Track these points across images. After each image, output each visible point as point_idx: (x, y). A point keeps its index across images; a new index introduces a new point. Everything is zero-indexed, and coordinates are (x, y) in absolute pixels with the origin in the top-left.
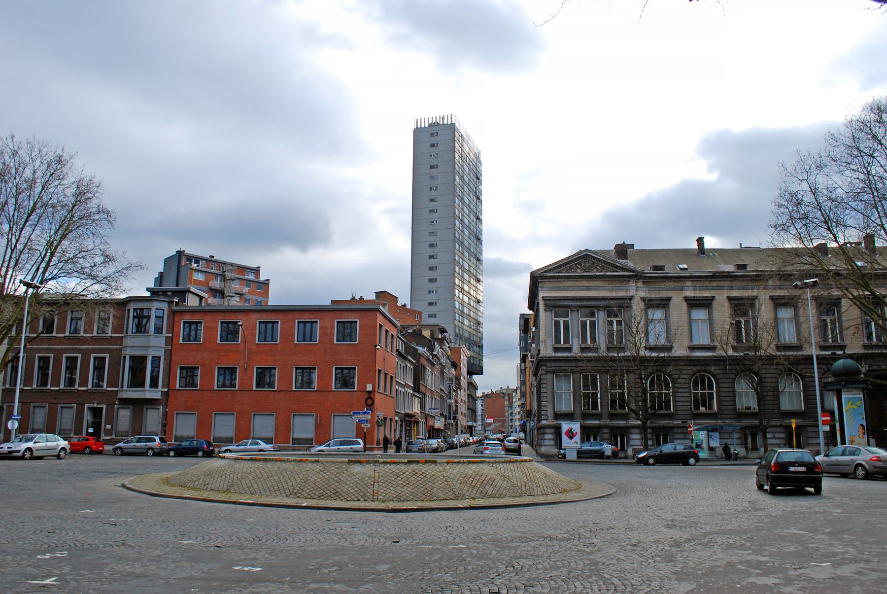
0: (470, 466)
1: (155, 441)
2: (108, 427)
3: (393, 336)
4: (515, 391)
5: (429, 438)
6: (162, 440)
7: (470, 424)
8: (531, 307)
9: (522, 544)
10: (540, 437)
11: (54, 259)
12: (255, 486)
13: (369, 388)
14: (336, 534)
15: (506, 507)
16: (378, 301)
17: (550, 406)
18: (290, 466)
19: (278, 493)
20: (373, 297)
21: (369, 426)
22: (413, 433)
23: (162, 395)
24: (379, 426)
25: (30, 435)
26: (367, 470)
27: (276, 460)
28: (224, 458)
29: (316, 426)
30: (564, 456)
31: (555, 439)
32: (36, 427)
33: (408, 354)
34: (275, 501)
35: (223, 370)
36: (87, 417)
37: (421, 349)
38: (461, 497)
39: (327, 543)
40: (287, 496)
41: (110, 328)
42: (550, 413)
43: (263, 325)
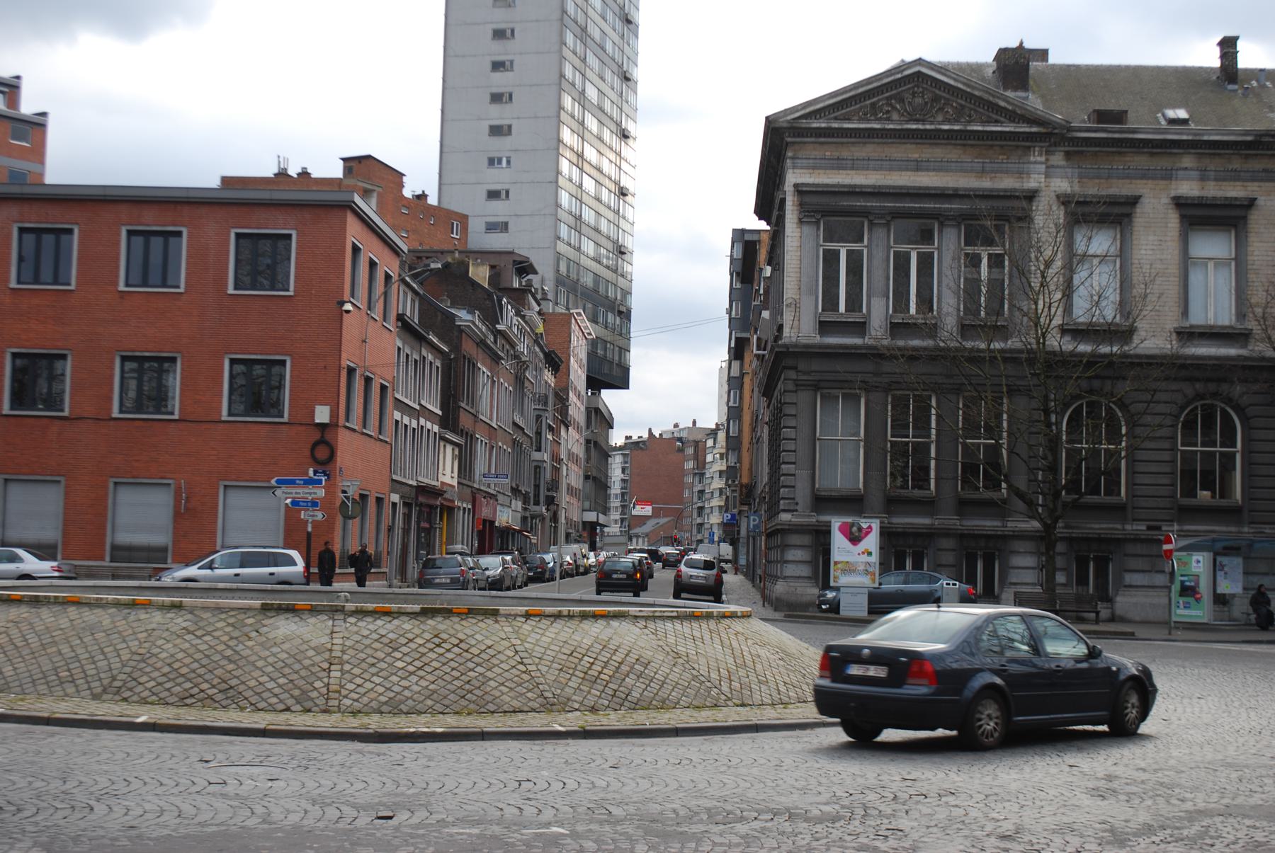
0: (586, 625)
3: (388, 277)
4: (713, 433)
5: (482, 551)
7: (591, 516)
8: (763, 209)
10: (775, 555)
13: (322, 414)
18: (104, 618)
20: (337, 171)
21: (319, 516)
22: (439, 538)
24: (347, 517)
29: (178, 515)
30: (835, 607)
31: (813, 563)
33: (428, 328)
34: (62, 709)
38: (563, 706)
40: (95, 697)
42: (802, 494)
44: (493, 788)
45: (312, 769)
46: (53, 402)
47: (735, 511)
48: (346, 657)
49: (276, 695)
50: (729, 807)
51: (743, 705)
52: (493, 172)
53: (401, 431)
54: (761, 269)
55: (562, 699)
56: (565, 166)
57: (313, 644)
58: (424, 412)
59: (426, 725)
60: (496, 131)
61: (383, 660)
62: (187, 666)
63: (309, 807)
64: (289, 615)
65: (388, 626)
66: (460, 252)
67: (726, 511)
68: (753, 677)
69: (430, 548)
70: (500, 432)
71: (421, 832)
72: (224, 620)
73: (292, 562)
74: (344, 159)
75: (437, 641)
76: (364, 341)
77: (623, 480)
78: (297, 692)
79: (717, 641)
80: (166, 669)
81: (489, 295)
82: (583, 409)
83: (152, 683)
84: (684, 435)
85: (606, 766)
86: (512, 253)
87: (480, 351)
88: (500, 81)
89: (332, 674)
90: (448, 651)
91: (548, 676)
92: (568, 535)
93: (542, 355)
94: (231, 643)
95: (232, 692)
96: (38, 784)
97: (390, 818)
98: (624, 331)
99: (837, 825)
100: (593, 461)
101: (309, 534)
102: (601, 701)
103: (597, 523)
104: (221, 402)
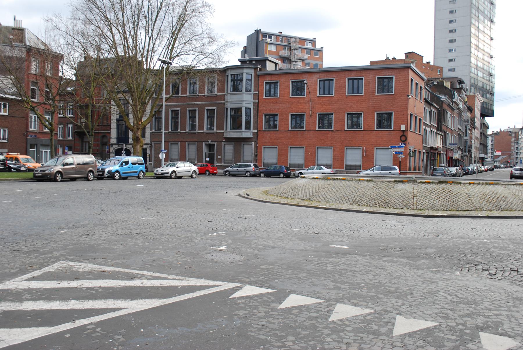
0: (488, 186)
1: (250, 166)
2: (219, 157)
3: (421, 87)
5: (449, 166)
6: (255, 166)
7: (482, 156)
11: (177, 42)
12: (328, 197)
13: (403, 128)
15: (516, 217)
16: (407, 60)
18: (352, 183)
19: (345, 202)
20: (403, 57)
21: (403, 156)
22: (437, 162)
24: (410, 157)
25: (173, 163)
26: (408, 188)
27: (342, 180)
28: (304, 177)
29: (363, 157)
32: (173, 157)
33: (433, 102)
34: (344, 207)
35: (295, 116)
36: (205, 150)
37: (443, 97)
38: (482, 210)
40: (351, 204)
41: (216, 89)
43: (322, 83)
52: (451, 53)
53: (425, 132)
56: (473, 50)
58: (432, 126)
60: (451, 41)
69: (434, 165)
73: (396, 169)
74: (406, 54)
77: (492, 145)
78: (405, 204)
81: (450, 91)
82: (479, 123)
84: (511, 130)
86: (457, 78)
88: (452, 26)
92: (475, 161)
100: (483, 139)
101: (400, 162)
103: (484, 158)
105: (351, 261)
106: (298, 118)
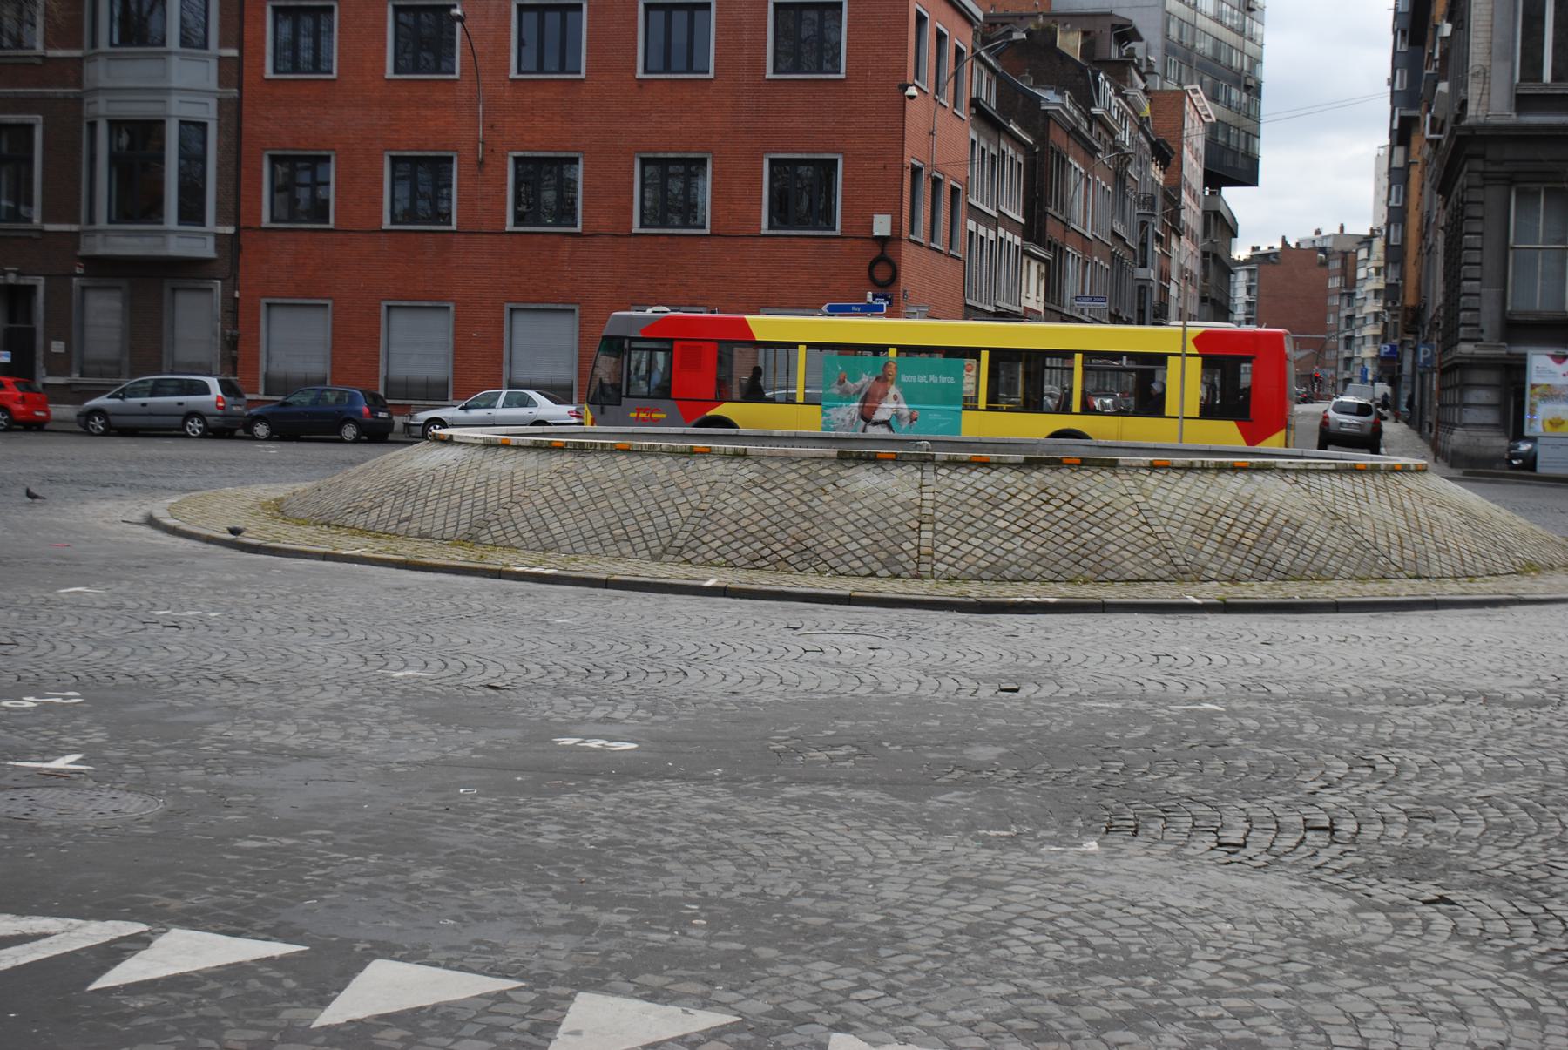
1: (205, 390)
2: (58, 347)
3: (959, 52)
4: (1367, 241)
6: (227, 388)
9: (1396, 710)
12: (555, 527)
13: (882, 226)
14: (825, 664)
17: (1490, 295)
18: (659, 468)
19: (627, 549)
23: (218, 246)
28: (449, 441)
30: (1530, 462)
31: (1501, 407)
34: (622, 571)
37: (1050, 98)
38: (1198, 575)
39: (805, 685)
40: (655, 558)
42: (1489, 318)
43: (531, 17)
44: (1128, 663)
45: (915, 639)
46: (565, 212)
47: (1396, 342)
48: (938, 515)
49: (859, 558)
50: (1410, 688)
51: (1418, 577)
53: (976, 244)
54: (1437, 27)
55: (1195, 567)
57: (899, 500)
58: (1003, 220)
59: (1035, 594)
61: (981, 519)
62: (756, 523)
63: (922, 678)
64: (870, 466)
65: (987, 479)
66: (1045, 16)
67: (1384, 342)
68: (1430, 544)
70: (1096, 243)
71: (1054, 705)
72: (796, 471)
75: (1044, 496)
76: (931, 134)
77: (1249, 304)
79: (1385, 499)
80: (733, 527)
81: (1083, 70)
82: (1199, 212)
83: (718, 543)
84: (1328, 243)
85: (1257, 642)
86: (1110, 15)
87: (1071, 143)
89: (923, 534)
90: (1058, 508)
91: (1178, 540)
93: (1148, 146)
94: (806, 498)
95: (808, 555)
96: (619, 647)
97: (1016, 691)
98: (1252, 112)
99: (1543, 710)
102: (1243, 570)
104: (760, 212)
105: (646, 804)
106: (424, 175)
